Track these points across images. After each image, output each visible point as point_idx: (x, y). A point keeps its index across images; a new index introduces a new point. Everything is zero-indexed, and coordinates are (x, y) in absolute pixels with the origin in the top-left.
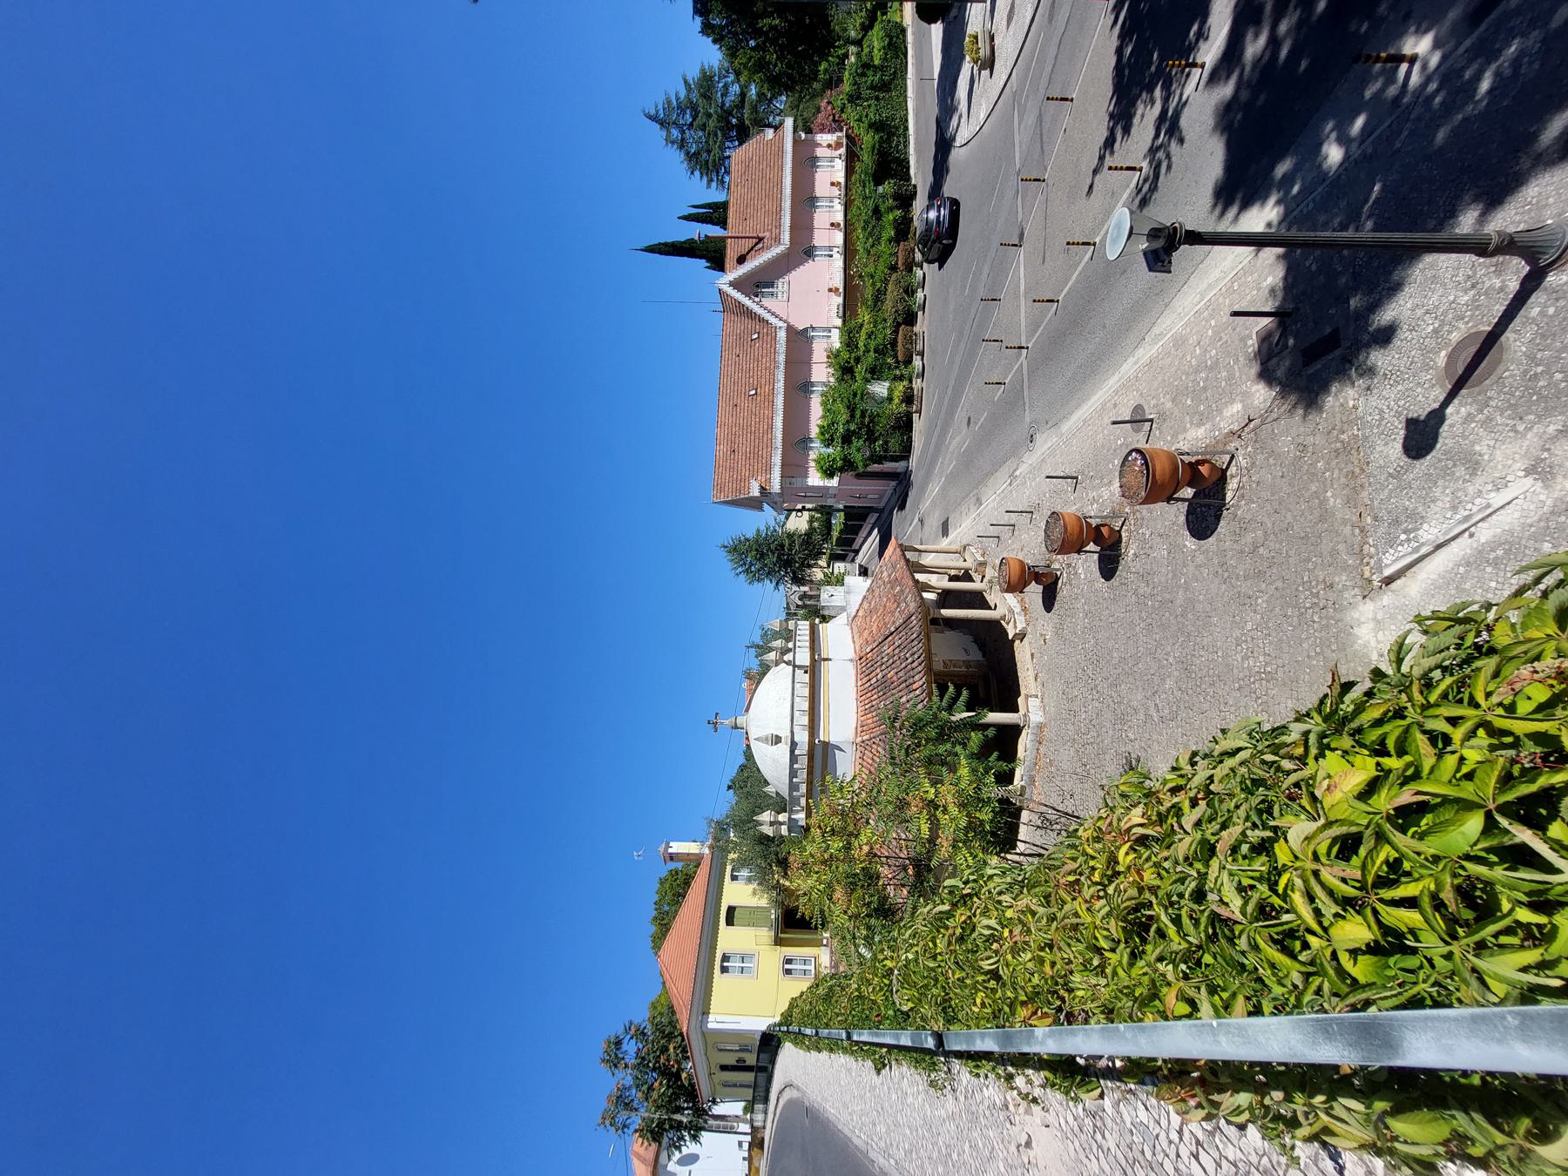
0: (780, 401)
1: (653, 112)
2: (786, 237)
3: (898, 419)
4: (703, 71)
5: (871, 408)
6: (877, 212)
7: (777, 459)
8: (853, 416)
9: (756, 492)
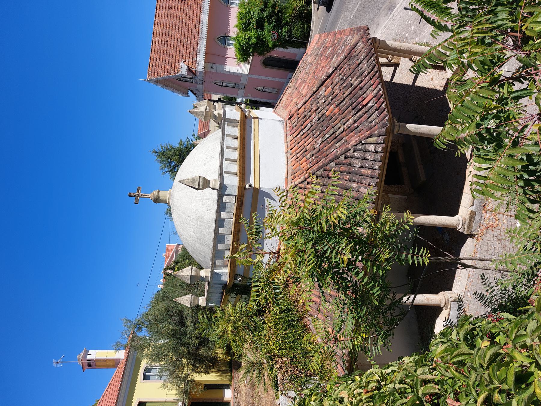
3: (301, 12)
7: (202, 46)
8: (266, 5)
9: (184, 71)
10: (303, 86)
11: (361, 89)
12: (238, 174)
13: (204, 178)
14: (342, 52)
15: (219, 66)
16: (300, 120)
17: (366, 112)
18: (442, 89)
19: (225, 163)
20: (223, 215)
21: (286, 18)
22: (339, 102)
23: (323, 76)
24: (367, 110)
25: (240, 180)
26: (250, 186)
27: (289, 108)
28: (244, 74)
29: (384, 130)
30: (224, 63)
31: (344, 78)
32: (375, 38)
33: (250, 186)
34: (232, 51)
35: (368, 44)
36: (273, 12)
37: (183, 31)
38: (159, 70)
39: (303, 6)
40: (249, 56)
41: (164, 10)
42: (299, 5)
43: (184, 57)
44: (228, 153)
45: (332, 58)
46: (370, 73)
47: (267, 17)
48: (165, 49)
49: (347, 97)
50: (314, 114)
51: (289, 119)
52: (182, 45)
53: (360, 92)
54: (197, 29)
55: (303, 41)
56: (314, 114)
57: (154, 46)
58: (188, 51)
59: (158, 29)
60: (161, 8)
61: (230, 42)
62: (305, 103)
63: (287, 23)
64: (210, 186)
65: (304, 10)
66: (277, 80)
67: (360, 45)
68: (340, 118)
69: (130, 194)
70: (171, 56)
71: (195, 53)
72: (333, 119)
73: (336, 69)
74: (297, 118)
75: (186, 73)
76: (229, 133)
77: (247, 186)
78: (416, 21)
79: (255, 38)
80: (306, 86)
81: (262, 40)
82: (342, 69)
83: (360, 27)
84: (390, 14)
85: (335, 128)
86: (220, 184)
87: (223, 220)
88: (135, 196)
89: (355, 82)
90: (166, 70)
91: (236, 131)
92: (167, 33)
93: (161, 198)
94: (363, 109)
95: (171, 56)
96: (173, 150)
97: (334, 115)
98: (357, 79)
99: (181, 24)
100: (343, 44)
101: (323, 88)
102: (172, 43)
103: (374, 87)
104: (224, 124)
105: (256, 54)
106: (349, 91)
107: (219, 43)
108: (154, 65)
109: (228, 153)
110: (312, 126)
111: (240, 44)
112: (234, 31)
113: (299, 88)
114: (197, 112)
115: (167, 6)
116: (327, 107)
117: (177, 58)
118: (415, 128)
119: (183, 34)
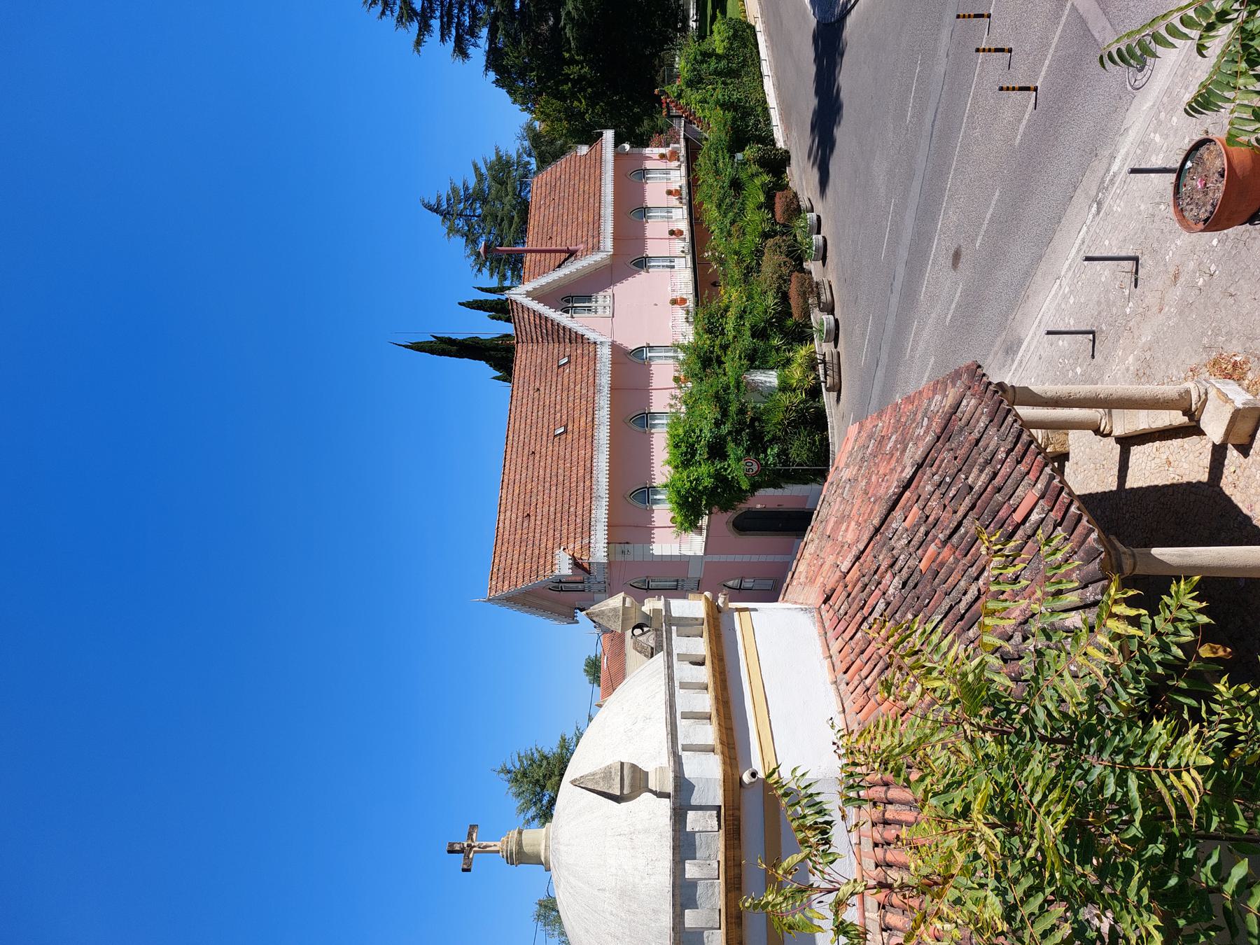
0: (603, 434)
1: (433, 202)
2: (608, 244)
3: (801, 414)
4: (499, 158)
5: (754, 403)
6: (736, 185)
7: (601, 513)
8: (725, 413)
9: (564, 567)
10: (844, 528)
11: (999, 490)
12: (718, 747)
13: (634, 767)
14: (924, 435)
15: (638, 547)
16: (854, 599)
17: (1029, 537)
18: (1204, 477)
19: (682, 724)
20: (692, 870)
21: (771, 429)
22: (948, 532)
23: (891, 491)
24: (1029, 532)
25: (724, 763)
26: (754, 775)
27: (820, 580)
28: (695, 557)
29: (1095, 565)
30: (649, 540)
31: (948, 479)
32: (1001, 385)
33: (754, 775)
34: (664, 512)
35: (989, 393)
36: (742, 422)
37: (560, 490)
38: (514, 574)
39: (805, 402)
40: (699, 515)
41: (519, 460)
42: (796, 401)
43: (564, 539)
44: (685, 701)
45: (904, 450)
46: (1012, 450)
47: (730, 433)
48: (525, 531)
49: (965, 516)
50: (888, 575)
51: (825, 602)
52: (558, 518)
53: (999, 497)
54: (588, 483)
55: (817, 466)
56: (888, 575)
57: (501, 530)
58: (572, 527)
59: (510, 496)
60: (514, 457)
61: (658, 497)
62: (858, 558)
63: (775, 439)
64: (652, 785)
65: (808, 409)
66: (770, 558)
67: (969, 404)
68: (960, 567)
69: (451, 845)
70: (537, 543)
71: (586, 529)
72: (941, 576)
73: (920, 466)
74: (845, 594)
75: (570, 572)
76: (683, 651)
77: (746, 778)
78: (1081, 357)
79: (709, 476)
80: (853, 523)
81: (725, 478)
82: (937, 462)
83: (956, 371)
84: (1013, 361)
85: (954, 593)
86: (676, 778)
87: (693, 884)
88: (462, 851)
89: (978, 479)
90: (527, 572)
91: (700, 646)
92: (528, 500)
93: (526, 849)
94: (1020, 532)
95: (537, 543)
96: (545, 763)
97: (942, 564)
98: (981, 471)
99: (554, 479)
100: (925, 415)
101: (898, 513)
102: (539, 518)
103: (1032, 476)
104: (669, 632)
105: (715, 509)
106: (968, 501)
107: (636, 503)
108: (502, 566)
109: (685, 701)
110: (888, 604)
111: (679, 492)
112: (662, 470)
113: (822, 556)
114: (603, 612)
115: (526, 452)
116: (920, 551)
117: (550, 545)
118: (1180, 556)
119: (560, 496)
